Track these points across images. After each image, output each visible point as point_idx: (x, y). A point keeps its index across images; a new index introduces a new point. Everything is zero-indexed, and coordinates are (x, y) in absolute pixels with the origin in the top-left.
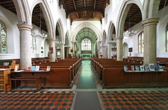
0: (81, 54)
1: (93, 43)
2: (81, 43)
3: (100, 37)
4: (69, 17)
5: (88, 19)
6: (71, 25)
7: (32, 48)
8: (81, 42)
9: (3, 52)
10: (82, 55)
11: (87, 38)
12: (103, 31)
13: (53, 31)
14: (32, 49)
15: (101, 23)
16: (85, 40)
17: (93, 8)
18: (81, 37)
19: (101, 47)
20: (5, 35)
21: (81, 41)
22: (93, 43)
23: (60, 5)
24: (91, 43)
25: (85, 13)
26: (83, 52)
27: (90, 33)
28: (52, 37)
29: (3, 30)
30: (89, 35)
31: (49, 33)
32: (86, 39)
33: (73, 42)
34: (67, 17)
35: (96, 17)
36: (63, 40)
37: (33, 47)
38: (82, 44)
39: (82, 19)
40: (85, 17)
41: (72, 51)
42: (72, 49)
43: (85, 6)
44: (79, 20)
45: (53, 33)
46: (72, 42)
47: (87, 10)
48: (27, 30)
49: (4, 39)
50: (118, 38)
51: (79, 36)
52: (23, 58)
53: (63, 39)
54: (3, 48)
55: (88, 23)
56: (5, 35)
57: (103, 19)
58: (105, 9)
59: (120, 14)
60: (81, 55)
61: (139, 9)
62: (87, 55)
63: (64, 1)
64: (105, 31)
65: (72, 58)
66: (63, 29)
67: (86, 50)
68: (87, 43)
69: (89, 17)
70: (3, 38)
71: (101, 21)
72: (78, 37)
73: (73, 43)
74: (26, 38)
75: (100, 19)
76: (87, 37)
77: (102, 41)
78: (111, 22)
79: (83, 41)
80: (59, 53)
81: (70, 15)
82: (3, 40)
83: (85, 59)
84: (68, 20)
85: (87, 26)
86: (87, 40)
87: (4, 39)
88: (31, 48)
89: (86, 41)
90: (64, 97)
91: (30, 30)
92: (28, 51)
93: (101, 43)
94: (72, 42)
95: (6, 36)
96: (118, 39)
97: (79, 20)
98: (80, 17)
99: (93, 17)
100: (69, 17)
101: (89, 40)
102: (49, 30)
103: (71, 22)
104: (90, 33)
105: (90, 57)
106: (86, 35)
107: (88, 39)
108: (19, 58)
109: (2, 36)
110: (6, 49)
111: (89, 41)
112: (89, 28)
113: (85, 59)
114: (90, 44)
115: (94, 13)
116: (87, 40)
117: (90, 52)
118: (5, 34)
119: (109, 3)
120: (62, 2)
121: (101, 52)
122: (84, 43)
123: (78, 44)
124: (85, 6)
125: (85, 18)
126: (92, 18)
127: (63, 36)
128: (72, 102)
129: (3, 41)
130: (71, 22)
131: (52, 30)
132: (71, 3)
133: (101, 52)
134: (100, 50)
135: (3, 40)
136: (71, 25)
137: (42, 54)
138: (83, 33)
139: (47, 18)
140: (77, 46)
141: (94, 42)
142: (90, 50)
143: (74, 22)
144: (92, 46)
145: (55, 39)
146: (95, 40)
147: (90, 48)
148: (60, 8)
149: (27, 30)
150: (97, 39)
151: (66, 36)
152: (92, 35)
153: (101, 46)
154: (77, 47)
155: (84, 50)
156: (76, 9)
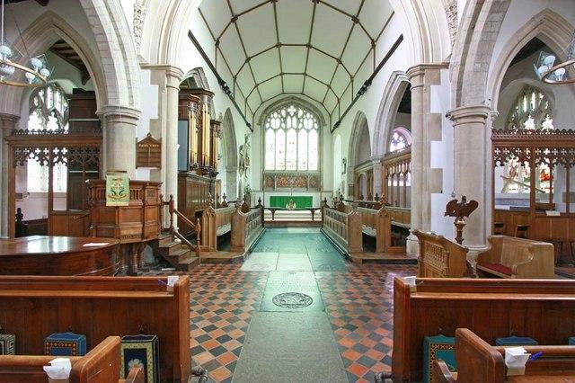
0: (263, 190)
1: (326, 129)
2: (264, 131)
8: (262, 123)
10: (268, 195)
11: (297, 106)
16: (288, 114)
19: (438, 119)
21: (265, 121)
22: (326, 129)
24: (320, 131)
26: (270, 180)
32: (292, 110)
38: (269, 134)
41: (149, 152)
42: (149, 139)
46: (155, 68)
60: (261, 195)
62: (295, 195)
67: (291, 168)
68: (297, 130)
76: (297, 100)
79: (275, 122)
83: (285, 225)
86: (296, 114)
89: (292, 122)
90: (216, 328)
93: (438, 82)
94: (150, 63)
99: (273, 186)
105: (313, 210)
106: (293, 84)
111: (309, 122)
113: (285, 225)
114: (314, 135)
116: (296, 114)
117: (314, 181)
121: (434, 164)
123: (241, 131)
128: (232, 370)
133: (434, 164)
134: (434, 144)
141: (337, 125)
142: (311, 169)
153: (436, 107)
155: (279, 168)
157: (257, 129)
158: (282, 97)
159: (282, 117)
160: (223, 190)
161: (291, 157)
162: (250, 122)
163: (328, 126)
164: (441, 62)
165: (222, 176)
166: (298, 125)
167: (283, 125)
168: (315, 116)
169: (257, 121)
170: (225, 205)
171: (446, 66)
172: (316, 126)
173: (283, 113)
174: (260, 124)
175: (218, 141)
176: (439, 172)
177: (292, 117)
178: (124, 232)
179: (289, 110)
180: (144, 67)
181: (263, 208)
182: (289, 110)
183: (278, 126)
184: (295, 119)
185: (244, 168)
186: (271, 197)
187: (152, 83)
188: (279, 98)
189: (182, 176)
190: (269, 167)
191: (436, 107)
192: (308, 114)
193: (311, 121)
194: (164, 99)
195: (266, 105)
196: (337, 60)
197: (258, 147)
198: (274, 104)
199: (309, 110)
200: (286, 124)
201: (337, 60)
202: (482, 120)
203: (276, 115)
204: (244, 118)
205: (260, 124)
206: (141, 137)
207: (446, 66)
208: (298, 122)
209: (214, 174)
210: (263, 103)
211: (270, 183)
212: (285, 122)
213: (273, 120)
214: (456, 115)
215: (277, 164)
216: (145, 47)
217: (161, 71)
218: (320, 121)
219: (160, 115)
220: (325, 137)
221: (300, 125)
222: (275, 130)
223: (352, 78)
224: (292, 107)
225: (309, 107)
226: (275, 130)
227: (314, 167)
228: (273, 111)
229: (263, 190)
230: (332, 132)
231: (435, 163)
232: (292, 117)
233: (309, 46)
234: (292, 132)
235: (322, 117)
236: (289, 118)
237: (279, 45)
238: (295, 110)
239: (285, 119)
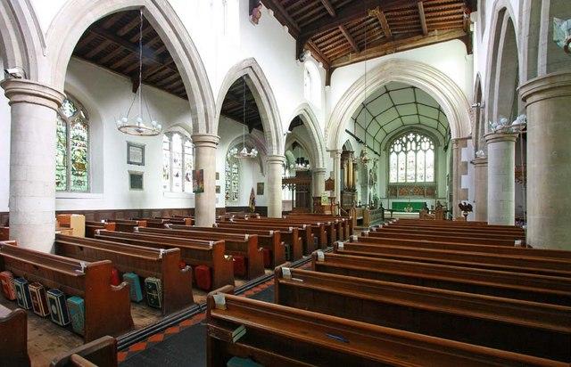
0: (388, 197)
1: (441, 149)
2: (389, 154)
3: (459, 117)
4: (308, 55)
5: (398, 45)
6: (328, 83)
7: (180, 174)
9: (73, 188)
10: (391, 201)
14: (180, 178)
15: (470, 51)
16: (408, 140)
18: (388, 128)
20: (86, 139)
24: (436, 150)
25: (383, 20)
26: (394, 190)
27: (422, 110)
29: (79, 125)
30: (424, 120)
32: (411, 136)
35: (440, 28)
37: (183, 171)
38: (393, 157)
39: (370, 53)
40: (385, 40)
41: (330, 185)
44: (360, 58)
46: (331, 151)
48: (26, 102)
49: (79, 150)
50: (536, 87)
52: (16, 212)
53: (274, 137)
54: (78, 175)
55: (397, 61)
56: (86, 139)
62: (411, 201)
65: (328, 213)
66: (272, 100)
68: (416, 151)
69: (406, 36)
70: (77, 148)
73: (334, 152)
74: (23, 135)
75: (463, 34)
76: (417, 129)
77: (474, 136)
80: (370, 190)
81: (313, 40)
82: (78, 154)
84: (312, 66)
85: (394, 78)
86: (415, 139)
87: (81, 148)
92: (31, 182)
93: (466, 146)
94: (330, 149)
95: (88, 142)
96: (535, 98)
97: (360, 58)
98: (361, 46)
100: (308, 55)
101: (425, 139)
104: (422, 110)
105: (392, 211)
107: (418, 138)
109: (75, 141)
110: (85, 179)
111: (426, 144)
112: (414, 88)
114: (431, 155)
116: (415, 139)
118: (84, 135)
122: (402, 153)
125: (386, 45)
126: (415, 38)
129: (76, 157)
130: (330, 71)
135: (78, 154)
136: (328, 83)
137: (217, 195)
142: (427, 180)
144: (440, 164)
145: (216, 140)
147: (431, 171)
153: (464, 159)
155: (401, 181)
156: (332, 14)
157: (384, 153)
158: (403, 128)
160: (359, 198)
161: (411, 172)
164: (467, 136)
165: (358, 189)
167: (404, 149)
168: (431, 139)
169: (383, 148)
170: (360, 206)
171: (470, 138)
172: (432, 147)
173: (404, 140)
175: (357, 173)
176: (466, 190)
177: (411, 142)
178: (431, 179)
181: (383, 210)
183: (400, 150)
184: (414, 143)
185: (372, 183)
186: (393, 203)
188: (401, 129)
189: (342, 193)
190: (393, 180)
191: (464, 159)
193: (428, 143)
195: (390, 135)
197: (384, 166)
198: (397, 134)
199: (426, 136)
203: (398, 141)
206: (327, 178)
207: (470, 138)
208: (417, 145)
209: (354, 190)
212: (406, 146)
213: (396, 146)
214: (475, 162)
216: (328, 144)
217: (334, 152)
218: (436, 142)
220: (440, 156)
221: (418, 148)
222: (398, 153)
226: (398, 153)
227: (431, 179)
228: (396, 139)
229: (388, 197)
231: (464, 186)
232: (411, 142)
234: (411, 154)
236: (409, 144)
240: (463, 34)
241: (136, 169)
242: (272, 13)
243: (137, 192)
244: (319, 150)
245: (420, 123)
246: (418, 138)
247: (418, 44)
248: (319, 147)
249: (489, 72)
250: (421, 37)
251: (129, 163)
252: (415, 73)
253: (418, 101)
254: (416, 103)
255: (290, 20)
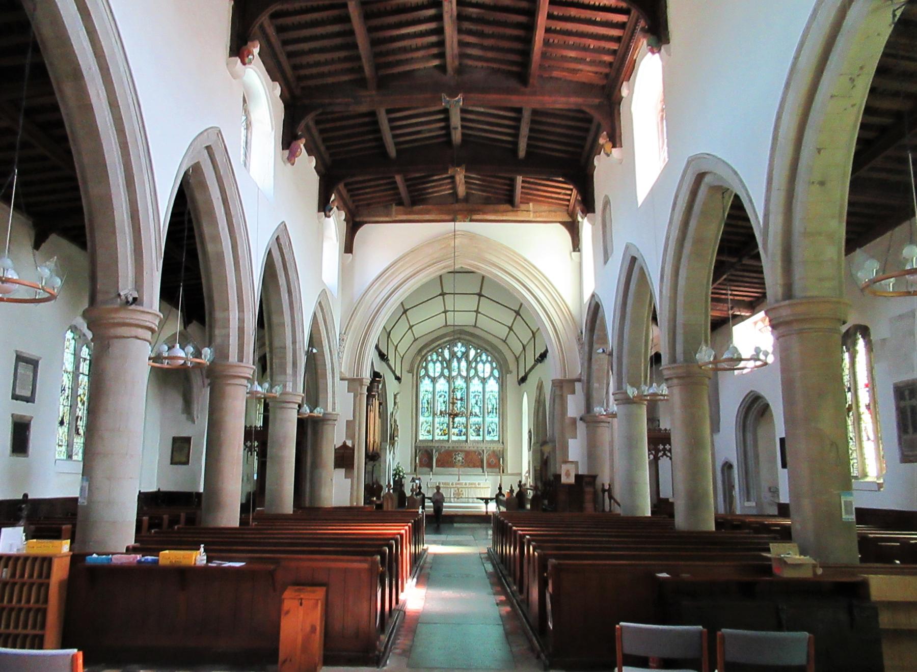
1: (512, 379)
6: (349, 248)
7: (66, 420)
11: (467, 344)
12: (587, 297)
13: (241, 321)
14: (65, 428)
16: (453, 355)
17: (515, 151)
18: (419, 331)
19: (574, 421)
23: (288, 140)
28: (233, 357)
30: (483, 322)
31: (217, 332)
32: (459, 349)
33: (360, 381)
34: (324, 206)
36: (289, 370)
38: (426, 385)
43: (457, 136)
45: (241, 330)
46: (351, 381)
47: (471, 164)
48: (291, 408)
51: (403, 326)
55: (472, 237)
57: (586, 227)
58: (596, 163)
59: (675, 233)
61: (753, 237)
63: (274, 16)
64: (634, 259)
69: (487, 201)
71: (573, 228)
72: (395, 338)
73: (354, 383)
77: (584, 378)
78: (700, 177)
86: (466, 355)
88: (62, 423)
91: (148, 335)
94: (347, 376)
102: (218, 315)
103: (353, 227)
106: (464, 319)
108: (74, 492)
114: (493, 386)
115: (519, 179)
116: (466, 355)
119: (615, 139)
120: (303, 124)
124: (457, 136)
127: (294, 342)
131: (234, 315)
132: (336, 28)
138: (437, 306)
139: (217, 239)
140: (383, 404)
141: (523, 380)
143: (368, 232)
146: (530, 362)
148: (291, 159)
149: (136, 337)
150: (543, 356)
151: (311, 344)
152: (508, 318)
154: (383, 415)
157: (407, 378)
159: (444, 359)
162: (398, 374)
163: (515, 372)
166: (468, 371)
168: (495, 359)
169: (406, 366)
171: (579, 380)
172: (496, 373)
173: (447, 354)
174: (410, 371)
177: (459, 360)
179: (456, 349)
180: (342, 379)
182: (456, 349)
184: (464, 364)
187: (348, 392)
192: (484, 357)
193: (488, 365)
194: (357, 405)
196: (515, 311)
198: (433, 341)
200: (450, 372)
201: (515, 311)
202: (607, 425)
204: (394, 372)
205: (410, 371)
210: (415, 340)
211: (425, 459)
212: (449, 367)
213: (431, 365)
215: (437, 431)
218: (503, 368)
219: (354, 417)
222: (434, 380)
223: (534, 334)
224: (459, 345)
225: (481, 343)
226: (434, 380)
230: (634, 259)
232: (459, 360)
233: (480, 295)
235: (506, 361)
236: (455, 364)
237: (443, 294)
238: (463, 349)
239: (449, 363)
240: (569, 220)
241: (22, 409)
242: (313, 161)
243: (21, 459)
244: (329, 376)
245: (475, 326)
246: (472, 353)
247: (504, 218)
248: (329, 371)
249: (618, 314)
250: (510, 207)
251: (15, 397)
252: (495, 260)
253: (514, 328)
254: (511, 329)
255: (322, 148)
